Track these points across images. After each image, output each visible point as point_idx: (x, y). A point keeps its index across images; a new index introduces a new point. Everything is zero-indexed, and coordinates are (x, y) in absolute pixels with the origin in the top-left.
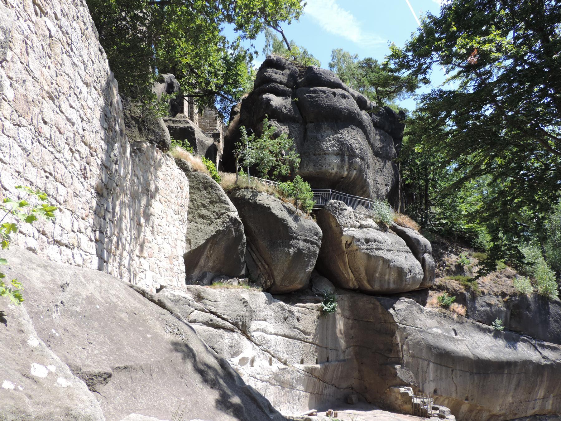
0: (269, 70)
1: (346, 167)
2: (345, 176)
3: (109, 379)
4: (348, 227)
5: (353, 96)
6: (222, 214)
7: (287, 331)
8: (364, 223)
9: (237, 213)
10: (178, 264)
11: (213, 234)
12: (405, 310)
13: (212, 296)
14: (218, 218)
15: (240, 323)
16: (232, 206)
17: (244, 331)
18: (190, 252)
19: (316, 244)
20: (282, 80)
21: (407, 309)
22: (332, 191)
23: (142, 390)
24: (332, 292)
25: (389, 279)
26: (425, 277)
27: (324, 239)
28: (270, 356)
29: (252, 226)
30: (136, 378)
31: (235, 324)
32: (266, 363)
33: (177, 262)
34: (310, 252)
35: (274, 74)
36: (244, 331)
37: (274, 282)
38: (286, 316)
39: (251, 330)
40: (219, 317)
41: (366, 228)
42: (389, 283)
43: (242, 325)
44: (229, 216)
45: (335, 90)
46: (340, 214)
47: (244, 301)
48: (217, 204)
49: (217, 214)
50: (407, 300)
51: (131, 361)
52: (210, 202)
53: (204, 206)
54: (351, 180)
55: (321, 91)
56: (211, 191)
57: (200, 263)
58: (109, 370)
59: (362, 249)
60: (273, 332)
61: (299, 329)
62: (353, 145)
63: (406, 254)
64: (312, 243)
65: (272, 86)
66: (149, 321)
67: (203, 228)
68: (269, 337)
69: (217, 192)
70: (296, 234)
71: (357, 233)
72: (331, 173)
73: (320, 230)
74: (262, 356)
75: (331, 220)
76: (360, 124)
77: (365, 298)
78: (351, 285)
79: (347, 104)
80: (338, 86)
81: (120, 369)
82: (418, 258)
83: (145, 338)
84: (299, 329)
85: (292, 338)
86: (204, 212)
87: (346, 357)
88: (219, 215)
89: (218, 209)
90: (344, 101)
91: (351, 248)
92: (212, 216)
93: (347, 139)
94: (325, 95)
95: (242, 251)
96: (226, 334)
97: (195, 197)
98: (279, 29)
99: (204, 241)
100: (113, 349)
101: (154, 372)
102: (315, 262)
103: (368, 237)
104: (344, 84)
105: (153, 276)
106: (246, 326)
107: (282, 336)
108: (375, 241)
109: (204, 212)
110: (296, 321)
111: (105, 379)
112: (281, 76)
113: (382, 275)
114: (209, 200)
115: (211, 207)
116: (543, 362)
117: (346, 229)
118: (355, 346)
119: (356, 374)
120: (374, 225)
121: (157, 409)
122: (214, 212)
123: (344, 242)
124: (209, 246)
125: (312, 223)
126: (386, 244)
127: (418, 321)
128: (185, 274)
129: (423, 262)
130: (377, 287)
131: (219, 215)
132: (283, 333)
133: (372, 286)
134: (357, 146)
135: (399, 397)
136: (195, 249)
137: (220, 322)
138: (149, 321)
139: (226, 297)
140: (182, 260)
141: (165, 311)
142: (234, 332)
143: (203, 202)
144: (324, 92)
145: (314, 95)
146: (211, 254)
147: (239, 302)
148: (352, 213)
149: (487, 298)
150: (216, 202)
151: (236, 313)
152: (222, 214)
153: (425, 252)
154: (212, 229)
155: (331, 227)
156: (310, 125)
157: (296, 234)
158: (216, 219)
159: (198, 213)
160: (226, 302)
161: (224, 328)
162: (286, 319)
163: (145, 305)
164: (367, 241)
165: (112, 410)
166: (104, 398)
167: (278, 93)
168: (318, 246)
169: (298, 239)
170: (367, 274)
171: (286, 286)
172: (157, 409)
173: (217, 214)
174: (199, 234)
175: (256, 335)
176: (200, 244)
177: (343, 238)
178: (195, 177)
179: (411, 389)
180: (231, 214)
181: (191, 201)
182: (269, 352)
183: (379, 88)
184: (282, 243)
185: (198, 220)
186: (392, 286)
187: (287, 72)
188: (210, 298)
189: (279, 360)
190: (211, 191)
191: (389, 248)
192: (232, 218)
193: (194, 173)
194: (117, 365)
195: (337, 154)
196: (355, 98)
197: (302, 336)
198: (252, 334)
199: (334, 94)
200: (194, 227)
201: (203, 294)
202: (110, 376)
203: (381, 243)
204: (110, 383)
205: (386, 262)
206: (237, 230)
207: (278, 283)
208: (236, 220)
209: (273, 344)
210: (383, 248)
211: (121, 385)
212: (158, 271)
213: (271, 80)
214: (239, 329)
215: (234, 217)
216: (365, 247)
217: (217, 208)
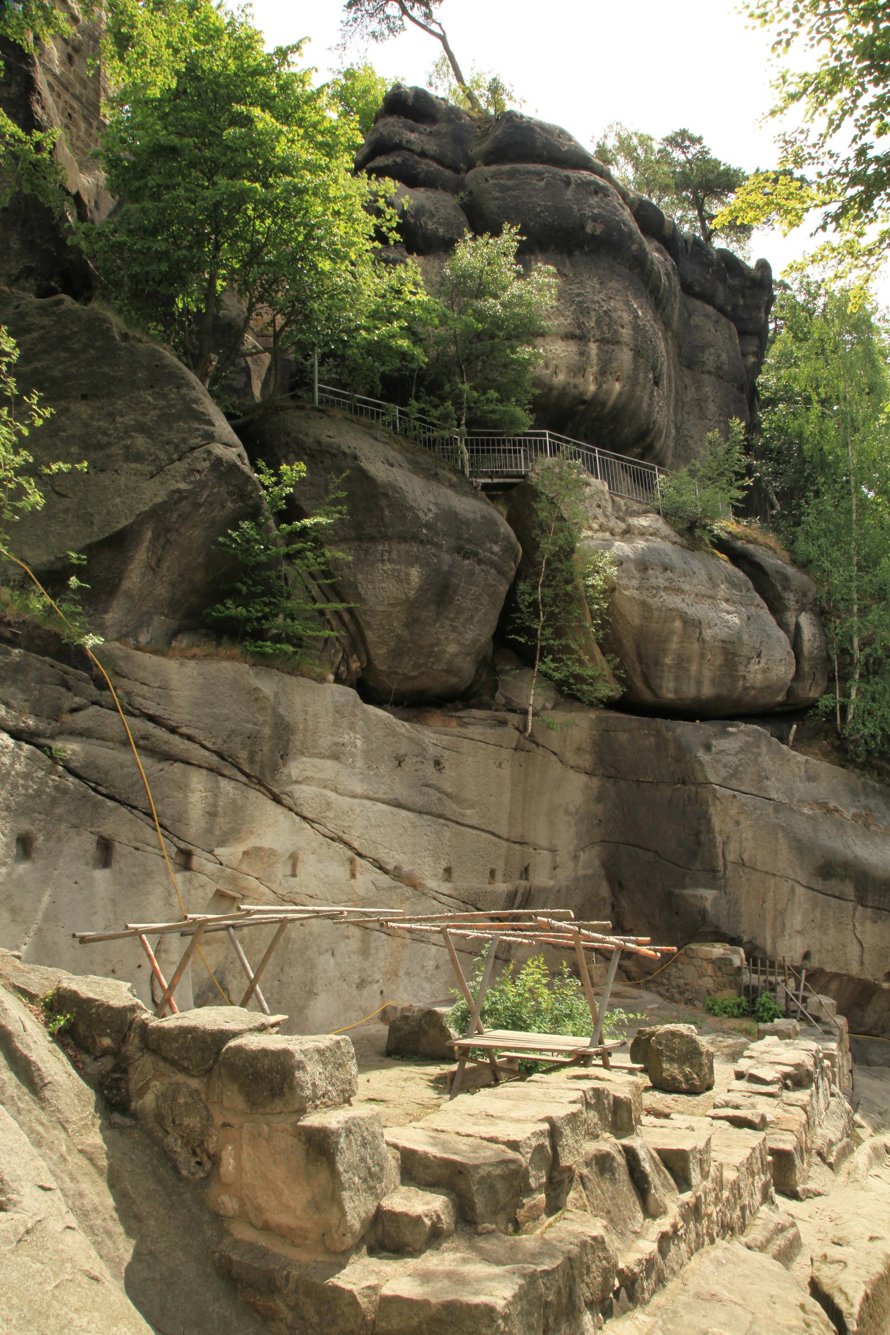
1: (592, 371)
2: (589, 396)
7: (402, 792)
12: (737, 754)
14: (180, 459)
16: (223, 426)
20: (426, 147)
21: (742, 750)
22: (550, 436)
24: (548, 705)
25: (700, 672)
28: (350, 854)
32: (340, 872)
38: (402, 752)
42: (699, 683)
44: (209, 453)
53: (141, 428)
54: (607, 410)
55: (529, 172)
57: (126, 585)
62: (615, 315)
65: (399, 160)
77: (634, 720)
79: (599, 207)
82: (782, 625)
87: (581, 872)
90: (594, 200)
98: (434, 27)
113: (682, 661)
124: (149, 535)
130: (668, 690)
132: (392, 796)
134: (626, 317)
135: (710, 969)
144: (539, 174)
145: (510, 183)
148: (607, 496)
150: (178, 417)
158: (172, 462)
162: (400, 762)
170: (640, 656)
171: (407, 678)
175: (305, 793)
179: (741, 950)
180: (218, 450)
182: (347, 844)
184: (390, 553)
186: (707, 691)
187: (442, 127)
188: (141, 675)
195: (568, 337)
199: (567, 182)
205: (692, 624)
207: (381, 665)
210: (686, 587)
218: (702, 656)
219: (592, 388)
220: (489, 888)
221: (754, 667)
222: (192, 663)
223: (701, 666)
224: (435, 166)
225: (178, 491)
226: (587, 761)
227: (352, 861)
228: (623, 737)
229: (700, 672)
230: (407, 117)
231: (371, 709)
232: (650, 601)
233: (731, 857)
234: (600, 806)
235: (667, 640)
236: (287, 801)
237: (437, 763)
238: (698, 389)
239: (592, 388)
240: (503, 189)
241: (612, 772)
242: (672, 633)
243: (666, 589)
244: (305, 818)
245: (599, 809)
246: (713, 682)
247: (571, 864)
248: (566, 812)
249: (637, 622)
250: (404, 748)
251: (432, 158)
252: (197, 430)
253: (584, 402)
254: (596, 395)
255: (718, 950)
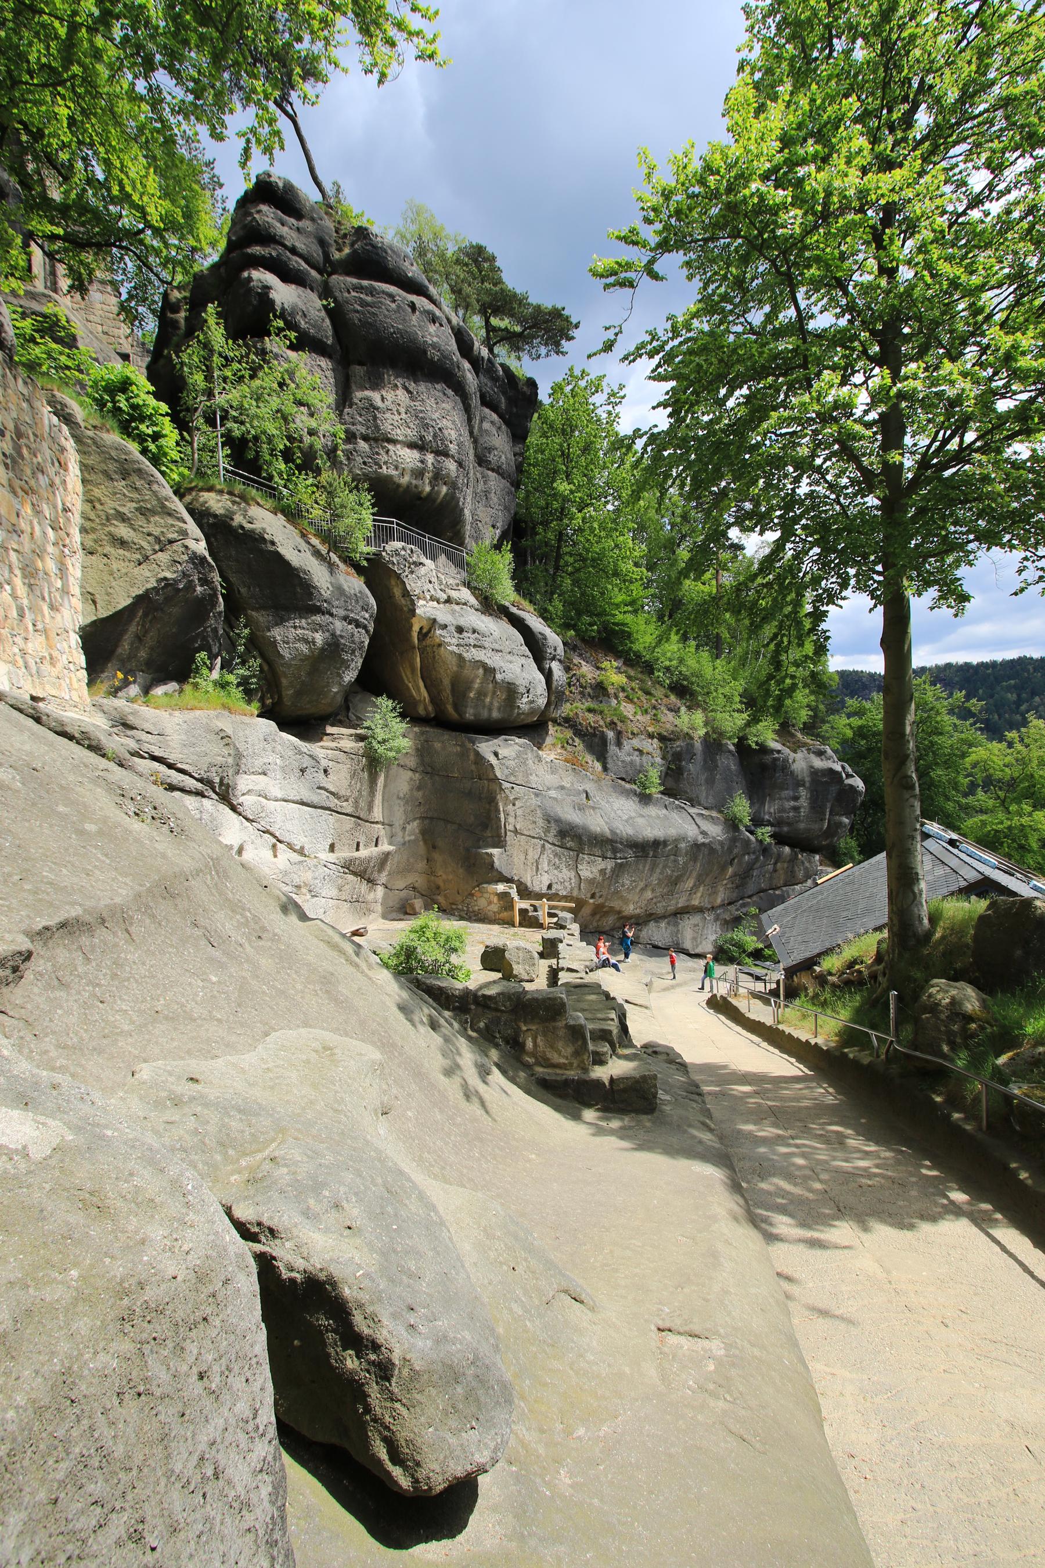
0: (264, 208)
3: (27, 964)
4: (425, 599)
5: (449, 321)
6: (171, 542)
7: (307, 795)
8: (454, 594)
9: (203, 544)
10: (67, 650)
11: (149, 586)
13: (154, 724)
14: (161, 550)
15: (217, 780)
17: (225, 795)
18: (94, 623)
19: (365, 627)
23: (114, 976)
25: (491, 703)
26: (548, 704)
27: (378, 620)
29: (233, 579)
30: (93, 947)
31: (209, 783)
33: (65, 644)
34: (353, 642)
35: (279, 225)
36: (225, 795)
37: (280, 697)
39: (238, 793)
40: (171, 766)
41: (458, 604)
42: (490, 710)
43: (221, 783)
45: (413, 298)
46: (412, 572)
47: (222, 734)
48: (157, 518)
49: (158, 540)
50: (517, 740)
51: (74, 903)
52: (137, 509)
53: (123, 518)
55: (383, 292)
56: (139, 484)
57: (120, 650)
58: (24, 944)
59: (450, 644)
60: (279, 796)
61: (326, 790)
62: (445, 432)
63: (523, 660)
64: (358, 625)
65: (274, 254)
66: (78, 789)
67: (124, 571)
68: (271, 805)
69: (155, 487)
70: (329, 603)
71: (442, 614)
72: (399, 486)
73: (372, 601)
74: (259, 841)
75: (393, 582)
76: (459, 388)
77: (446, 736)
78: (421, 711)
80: (419, 290)
81: (49, 934)
82: (541, 669)
83: (81, 833)
84: (326, 790)
85: (315, 807)
86: (123, 531)
87: (407, 838)
88: (163, 544)
89: (159, 530)
90: (432, 328)
91: (428, 641)
92: (144, 544)
93: (436, 416)
94: (393, 305)
95: (215, 630)
96: (190, 801)
97: (97, 492)
98: (289, 109)
99: (129, 601)
100: (10, 875)
101: (131, 924)
102: (359, 664)
103: (462, 622)
104: (433, 290)
105: (9, 673)
106: (228, 786)
107: (294, 802)
108: (474, 632)
109: (123, 531)
110: (321, 774)
111: (15, 969)
112: (294, 234)
114: (134, 505)
115: (141, 521)
116: (701, 839)
117: (421, 602)
118: (422, 818)
119: (421, 865)
120: (473, 601)
121: (166, 1018)
122: (149, 535)
123: (416, 628)
124: (140, 613)
125: (355, 584)
126: (491, 639)
127: (533, 778)
128: (85, 673)
129: (548, 676)
130: (470, 714)
131: (163, 544)
132: (298, 798)
133: (460, 715)
135: (495, 899)
136: (108, 618)
137: (176, 777)
138: (78, 789)
139: (185, 726)
140: (75, 640)
141: (103, 763)
142: (204, 796)
143: (121, 509)
144: (392, 297)
145: (369, 299)
146: (146, 632)
147: (213, 737)
149: (636, 742)
150: (153, 512)
151: (208, 759)
152: (171, 542)
153: (553, 659)
154: (148, 574)
155: (391, 597)
156: (358, 370)
157: (329, 603)
158: (155, 552)
159: (110, 534)
160: (184, 737)
161: (182, 790)
163: (51, 745)
164: (460, 630)
165: (53, 1054)
166: (21, 1024)
167: (288, 276)
168: (367, 631)
169: (331, 615)
170: (453, 690)
172: (166, 1018)
173: (158, 540)
174: (114, 584)
175: (248, 802)
176: (120, 607)
177: (414, 620)
178: (95, 443)
181: (90, 501)
183: (495, 321)
185: (108, 549)
186: (495, 714)
187: (305, 224)
188: (148, 726)
189: (290, 846)
190: (139, 484)
191: (497, 647)
192: (194, 553)
193: (90, 433)
194: (40, 923)
196: (452, 328)
197: (333, 802)
198: (241, 799)
199: (413, 307)
200: (101, 566)
201: (131, 720)
202: (28, 956)
203: (484, 636)
204: (29, 976)
205: (490, 671)
206: (205, 581)
207: (287, 701)
208: (203, 559)
209: (279, 818)
210: (487, 645)
211: (60, 974)
212: (21, 662)
213: (268, 238)
214: (215, 792)
215: (199, 552)
216: (454, 641)
217: (157, 525)
218: (494, 693)
219: (428, 489)
220: (356, 854)
221: (525, 700)
222: (177, 713)
223: (492, 698)
224: (304, 265)
225: (165, 579)
226: (412, 762)
227: (274, 846)
228: (438, 745)
229: (491, 703)
230: (277, 208)
231: (284, 735)
232: (465, 655)
233: (510, 827)
234: (420, 793)
235: (473, 682)
236: (240, 809)
237: (325, 771)
238: (485, 483)
239: (428, 489)
240: (363, 303)
241: (429, 770)
242: (477, 676)
243: (475, 646)
244: (247, 819)
245: (419, 794)
246: (499, 709)
247: (400, 834)
248: (399, 798)
249: (455, 668)
250: (307, 762)
251: (301, 256)
252: (173, 526)
253: (420, 498)
254: (430, 494)
255: (501, 887)
